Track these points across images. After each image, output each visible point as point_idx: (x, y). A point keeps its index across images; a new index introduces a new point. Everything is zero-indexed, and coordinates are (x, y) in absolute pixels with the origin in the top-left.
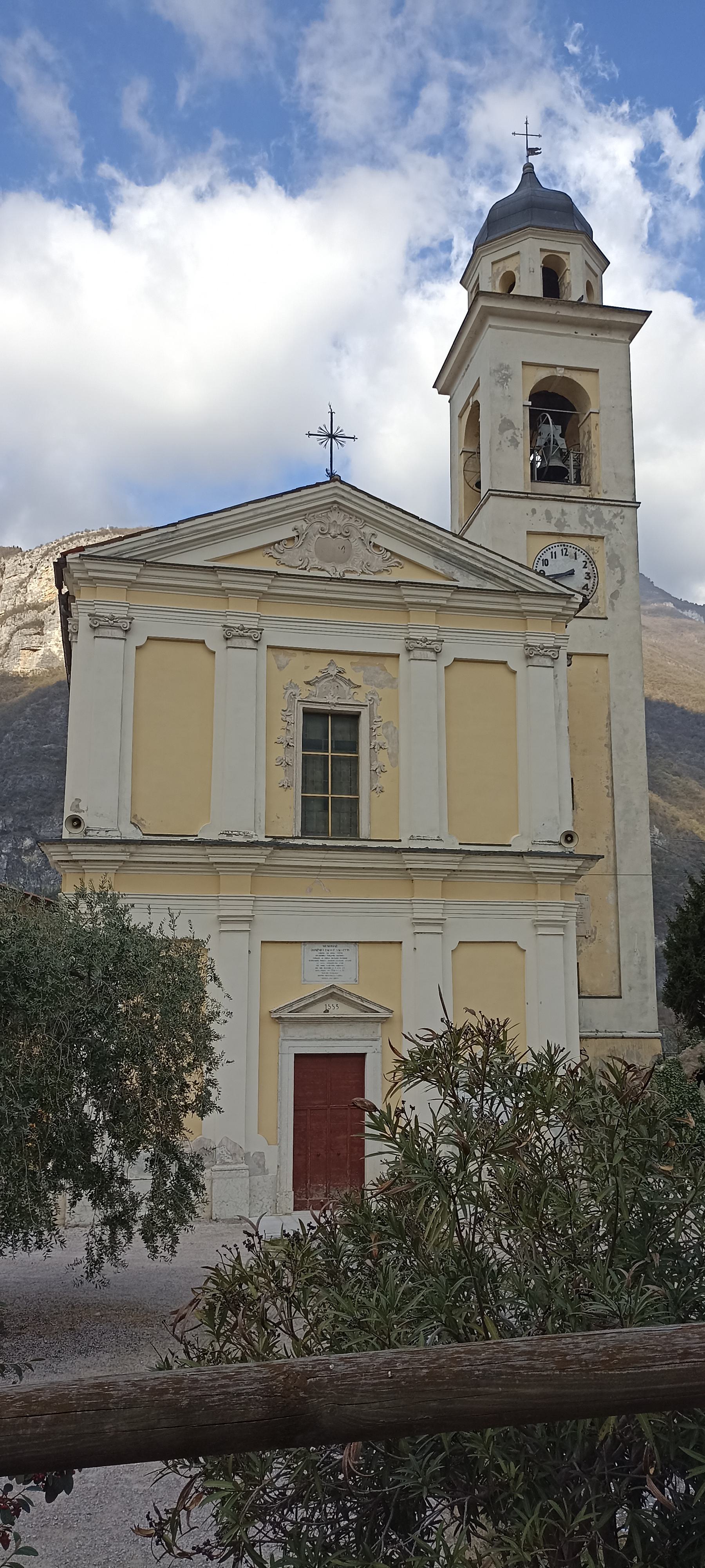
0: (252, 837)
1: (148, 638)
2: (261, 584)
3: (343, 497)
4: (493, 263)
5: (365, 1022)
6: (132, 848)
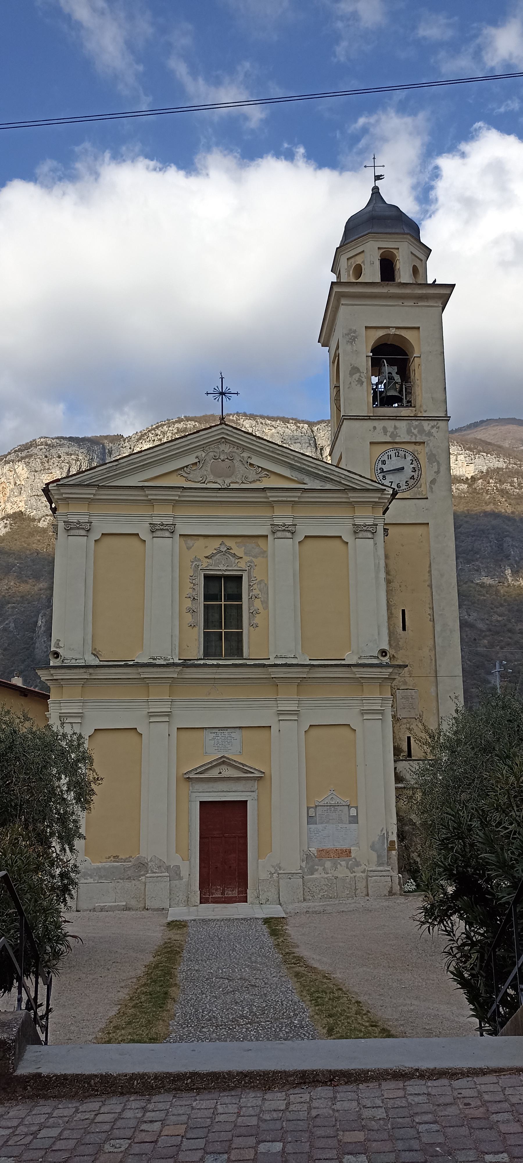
0: (169, 660)
1: (102, 534)
2: (174, 495)
3: (228, 435)
4: (348, 259)
5: (246, 780)
6: (91, 670)
